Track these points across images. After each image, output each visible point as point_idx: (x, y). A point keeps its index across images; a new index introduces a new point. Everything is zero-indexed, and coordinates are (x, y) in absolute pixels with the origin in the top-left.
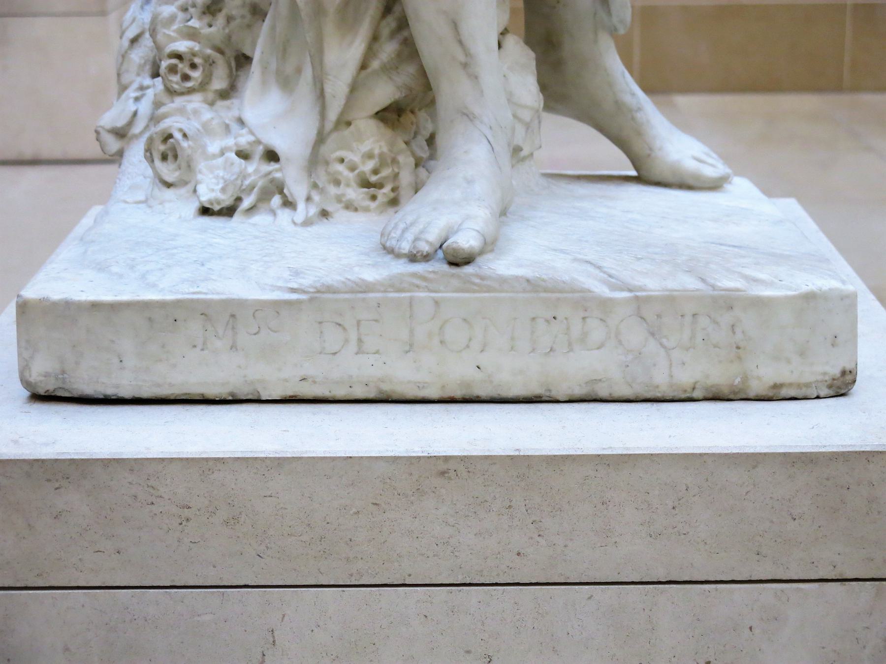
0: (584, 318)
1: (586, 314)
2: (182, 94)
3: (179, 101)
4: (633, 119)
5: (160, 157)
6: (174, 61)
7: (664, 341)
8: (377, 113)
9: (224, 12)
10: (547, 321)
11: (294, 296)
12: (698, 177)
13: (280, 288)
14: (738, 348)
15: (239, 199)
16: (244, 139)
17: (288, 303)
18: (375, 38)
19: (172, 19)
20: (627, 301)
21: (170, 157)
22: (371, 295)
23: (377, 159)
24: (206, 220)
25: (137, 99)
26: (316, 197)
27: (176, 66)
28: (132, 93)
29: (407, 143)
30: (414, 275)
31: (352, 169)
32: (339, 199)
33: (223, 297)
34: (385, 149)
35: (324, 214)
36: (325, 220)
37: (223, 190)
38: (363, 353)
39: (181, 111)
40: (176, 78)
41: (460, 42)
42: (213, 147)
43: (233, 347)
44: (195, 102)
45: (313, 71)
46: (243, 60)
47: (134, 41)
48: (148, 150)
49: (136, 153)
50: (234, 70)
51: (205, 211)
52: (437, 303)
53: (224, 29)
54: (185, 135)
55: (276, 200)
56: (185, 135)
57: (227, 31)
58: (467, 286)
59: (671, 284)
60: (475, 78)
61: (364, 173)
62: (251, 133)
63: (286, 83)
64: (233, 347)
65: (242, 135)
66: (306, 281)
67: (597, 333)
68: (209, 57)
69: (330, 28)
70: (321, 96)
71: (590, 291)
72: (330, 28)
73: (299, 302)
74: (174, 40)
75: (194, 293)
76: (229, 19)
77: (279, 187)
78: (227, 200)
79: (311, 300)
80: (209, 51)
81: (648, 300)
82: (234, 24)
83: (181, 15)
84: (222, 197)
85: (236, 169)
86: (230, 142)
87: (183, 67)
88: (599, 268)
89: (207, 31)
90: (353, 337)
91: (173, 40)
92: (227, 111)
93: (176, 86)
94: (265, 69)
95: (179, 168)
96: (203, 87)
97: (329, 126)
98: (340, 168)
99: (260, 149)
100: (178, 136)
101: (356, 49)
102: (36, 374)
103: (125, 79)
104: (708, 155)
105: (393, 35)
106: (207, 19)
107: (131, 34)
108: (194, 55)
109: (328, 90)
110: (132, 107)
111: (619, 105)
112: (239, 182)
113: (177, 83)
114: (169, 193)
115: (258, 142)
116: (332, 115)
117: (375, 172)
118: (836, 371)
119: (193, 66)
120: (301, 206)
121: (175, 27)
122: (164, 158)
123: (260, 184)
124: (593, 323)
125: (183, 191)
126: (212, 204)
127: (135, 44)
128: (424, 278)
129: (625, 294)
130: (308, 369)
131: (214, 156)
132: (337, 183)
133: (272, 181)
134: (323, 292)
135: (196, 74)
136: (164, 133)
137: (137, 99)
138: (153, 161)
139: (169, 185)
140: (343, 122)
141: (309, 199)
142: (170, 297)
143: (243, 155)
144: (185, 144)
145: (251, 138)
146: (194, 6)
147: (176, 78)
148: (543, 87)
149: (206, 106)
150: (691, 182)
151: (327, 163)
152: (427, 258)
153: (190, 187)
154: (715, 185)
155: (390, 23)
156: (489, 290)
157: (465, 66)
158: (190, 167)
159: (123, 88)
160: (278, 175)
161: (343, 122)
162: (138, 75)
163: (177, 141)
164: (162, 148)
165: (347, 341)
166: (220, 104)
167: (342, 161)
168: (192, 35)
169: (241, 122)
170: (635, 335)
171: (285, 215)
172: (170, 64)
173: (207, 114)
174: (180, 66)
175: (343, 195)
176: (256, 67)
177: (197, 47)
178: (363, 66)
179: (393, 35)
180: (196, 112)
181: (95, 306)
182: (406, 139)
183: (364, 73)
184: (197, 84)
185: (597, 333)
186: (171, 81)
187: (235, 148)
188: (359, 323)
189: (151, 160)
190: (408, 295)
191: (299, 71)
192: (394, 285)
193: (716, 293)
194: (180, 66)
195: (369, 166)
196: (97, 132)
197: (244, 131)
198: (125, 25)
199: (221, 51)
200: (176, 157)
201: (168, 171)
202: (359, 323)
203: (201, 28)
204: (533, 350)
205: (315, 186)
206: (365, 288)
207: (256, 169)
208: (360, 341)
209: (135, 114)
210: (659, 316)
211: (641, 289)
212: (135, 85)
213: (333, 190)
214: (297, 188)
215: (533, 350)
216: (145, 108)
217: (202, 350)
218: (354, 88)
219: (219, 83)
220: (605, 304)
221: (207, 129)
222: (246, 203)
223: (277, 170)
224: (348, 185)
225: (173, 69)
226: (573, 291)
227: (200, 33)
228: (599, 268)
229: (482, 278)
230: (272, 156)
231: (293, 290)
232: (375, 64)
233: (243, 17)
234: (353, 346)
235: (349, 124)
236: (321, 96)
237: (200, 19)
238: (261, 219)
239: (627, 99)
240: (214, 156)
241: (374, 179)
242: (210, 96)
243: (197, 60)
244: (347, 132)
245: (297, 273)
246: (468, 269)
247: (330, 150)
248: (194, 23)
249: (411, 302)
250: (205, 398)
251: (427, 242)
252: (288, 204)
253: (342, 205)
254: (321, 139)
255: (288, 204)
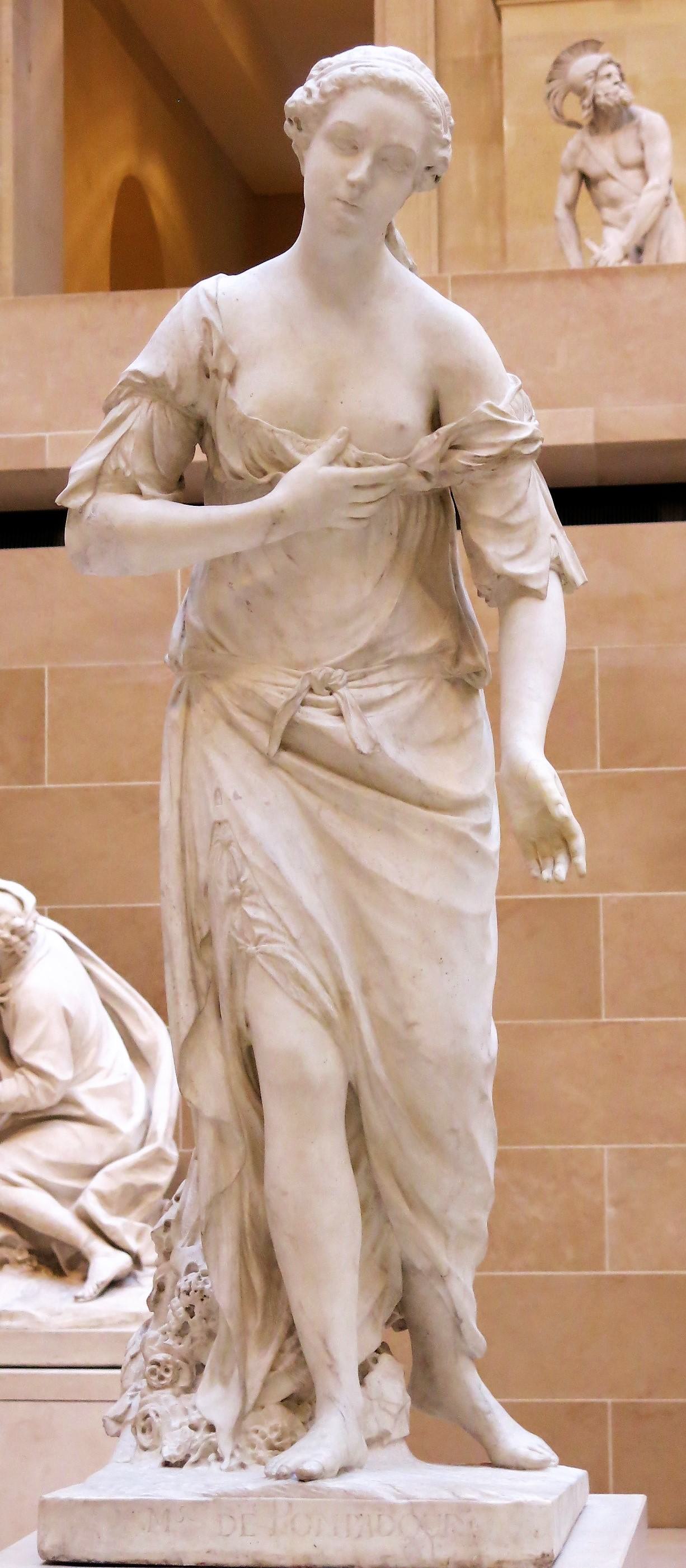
0: (380, 1515)
1: (381, 1513)
2: (158, 1389)
3: (156, 1393)
4: (485, 1419)
5: (141, 1429)
6: (154, 1366)
7: (430, 1532)
8: (282, 1401)
9: (188, 1336)
10: (356, 1517)
11: (204, 1499)
12: (527, 1460)
13: (197, 1494)
14: (475, 1536)
15: (188, 1456)
16: (194, 1417)
17: (202, 1503)
18: (281, 1351)
19: (156, 1339)
20: (406, 1505)
21: (147, 1431)
22: (250, 1499)
23: (280, 1431)
24: (167, 1469)
25: (132, 1397)
26: (237, 1454)
27: (155, 1369)
28: (129, 1393)
29: (304, 1423)
30: (278, 1487)
31: (264, 1437)
32: (254, 1457)
33: (163, 1498)
34: (286, 1425)
35: (243, 1466)
36: (243, 1470)
37: (178, 1449)
38: (245, 1535)
39: (157, 1400)
40: (155, 1378)
41: (328, 1352)
42: (175, 1423)
43: (167, 1530)
44: (167, 1394)
45: (239, 1370)
46: (200, 1368)
47: (133, 1357)
48: (134, 1427)
49: (127, 1432)
50: (195, 1374)
51: (167, 1464)
52: (290, 1504)
53: (189, 1346)
54: (157, 1415)
55: (212, 1456)
56: (157, 1415)
57: (190, 1348)
58: (308, 1494)
59: (434, 1496)
60: (337, 1375)
61: (270, 1439)
62: (200, 1412)
63: (225, 1381)
64: (167, 1530)
65: (193, 1414)
66: (212, 1490)
67: (388, 1526)
68: (178, 1364)
69: (252, 1343)
70: (244, 1387)
71: (383, 1498)
72: (252, 1343)
73: (207, 1502)
74: (156, 1353)
75: (145, 1495)
76: (192, 1340)
77: (213, 1448)
78: (180, 1455)
79: (214, 1501)
80: (178, 1361)
81: (419, 1505)
82: (195, 1344)
83: (161, 1337)
84: (177, 1453)
85: (188, 1436)
86: (186, 1419)
87: (160, 1371)
88: (394, 1487)
89: (177, 1347)
90: (239, 1525)
91: (153, 1352)
92: (186, 1400)
93: (155, 1384)
94: (212, 1373)
95: (152, 1438)
96: (173, 1384)
97: (249, 1408)
98: (255, 1436)
99: (204, 1423)
100: (153, 1415)
101: (268, 1358)
102: (47, 1547)
103: (126, 1383)
104: (540, 1446)
105: (292, 1350)
106: (179, 1339)
107: (132, 1353)
108: (168, 1362)
109: (249, 1384)
110: (129, 1403)
111: (476, 1410)
112: (189, 1444)
113: (155, 1381)
114: (147, 1453)
115: (203, 1419)
116: (251, 1401)
117: (279, 1439)
118: (539, 1554)
119: (167, 1370)
120: (227, 1460)
121: (157, 1344)
122: (144, 1431)
123: (203, 1445)
124: (384, 1518)
125: (154, 1453)
126: (171, 1459)
127: (134, 1359)
128: (283, 1489)
129: (405, 1501)
130: (212, 1545)
131: (175, 1429)
132: (253, 1446)
133: (211, 1443)
134: (223, 1496)
135: (168, 1376)
136: (144, 1414)
137: (132, 1397)
138: (136, 1434)
139: (145, 1449)
140: (258, 1406)
141: (232, 1455)
142: (131, 1498)
143: (194, 1428)
144: (157, 1420)
145: (199, 1416)
146: (170, 1331)
147: (155, 1378)
148: (412, 1388)
149: (174, 1397)
150: (523, 1464)
151: (247, 1433)
152: (285, 1477)
153: (158, 1450)
154: (539, 1466)
155: (290, 1343)
156: (321, 1496)
157: (330, 1367)
158: (159, 1436)
159: (124, 1390)
160: (213, 1440)
161: (258, 1406)
162: (135, 1380)
163: (152, 1418)
164: (142, 1424)
165: (235, 1528)
166: (184, 1396)
167: (257, 1431)
168: (167, 1349)
169: (195, 1407)
170: (411, 1527)
171: (215, 1466)
172: (151, 1369)
173: (173, 1401)
174: (158, 1370)
175: (256, 1454)
176: (206, 1372)
177: (169, 1357)
178: (272, 1369)
179: (292, 1350)
180: (166, 1400)
181: (86, 1503)
182: (303, 1421)
183: (273, 1373)
184: (169, 1382)
185: (388, 1526)
186: (151, 1380)
187: (188, 1423)
188: (243, 1516)
189: (135, 1434)
190: (272, 1499)
191: (232, 1372)
192: (266, 1493)
193: (460, 1501)
194: (158, 1370)
195: (275, 1435)
196: (104, 1421)
197: (195, 1412)
198: (128, 1347)
199: (186, 1361)
200: (151, 1430)
201: (145, 1440)
202: (243, 1516)
203: (174, 1345)
204: (348, 1536)
205: (237, 1447)
206: (248, 1494)
207: (201, 1437)
208: (243, 1528)
209: (130, 1406)
210: (425, 1516)
211: (413, 1498)
212: (132, 1388)
213: (250, 1451)
214: (225, 1448)
215: (348, 1536)
216: (136, 1402)
217: (148, 1531)
218: (265, 1384)
219: (184, 1382)
220: (392, 1507)
221: (173, 1412)
222: (193, 1459)
223: (213, 1437)
224: (260, 1449)
225: (153, 1372)
226: (373, 1498)
227: (173, 1349)
228: (394, 1487)
229: (317, 1489)
230: (211, 1428)
231: (205, 1495)
232: (281, 1368)
233: (202, 1338)
234: (239, 1531)
235: (263, 1407)
236: (244, 1387)
237: (173, 1339)
238: (201, 1468)
239: (482, 1405)
240: (175, 1429)
241: (277, 1444)
242: (177, 1390)
243: (170, 1366)
244: (261, 1413)
245: (208, 1486)
246: (310, 1484)
247: (249, 1424)
248: (170, 1342)
249: (274, 1504)
250: (149, 1563)
251: (287, 1467)
252: (220, 1459)
253: (255, 1461)
254: (242, 1417)
255: (220, 1459)
